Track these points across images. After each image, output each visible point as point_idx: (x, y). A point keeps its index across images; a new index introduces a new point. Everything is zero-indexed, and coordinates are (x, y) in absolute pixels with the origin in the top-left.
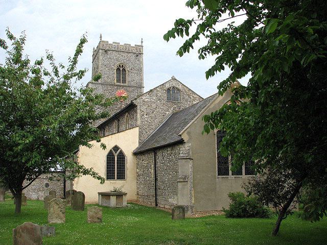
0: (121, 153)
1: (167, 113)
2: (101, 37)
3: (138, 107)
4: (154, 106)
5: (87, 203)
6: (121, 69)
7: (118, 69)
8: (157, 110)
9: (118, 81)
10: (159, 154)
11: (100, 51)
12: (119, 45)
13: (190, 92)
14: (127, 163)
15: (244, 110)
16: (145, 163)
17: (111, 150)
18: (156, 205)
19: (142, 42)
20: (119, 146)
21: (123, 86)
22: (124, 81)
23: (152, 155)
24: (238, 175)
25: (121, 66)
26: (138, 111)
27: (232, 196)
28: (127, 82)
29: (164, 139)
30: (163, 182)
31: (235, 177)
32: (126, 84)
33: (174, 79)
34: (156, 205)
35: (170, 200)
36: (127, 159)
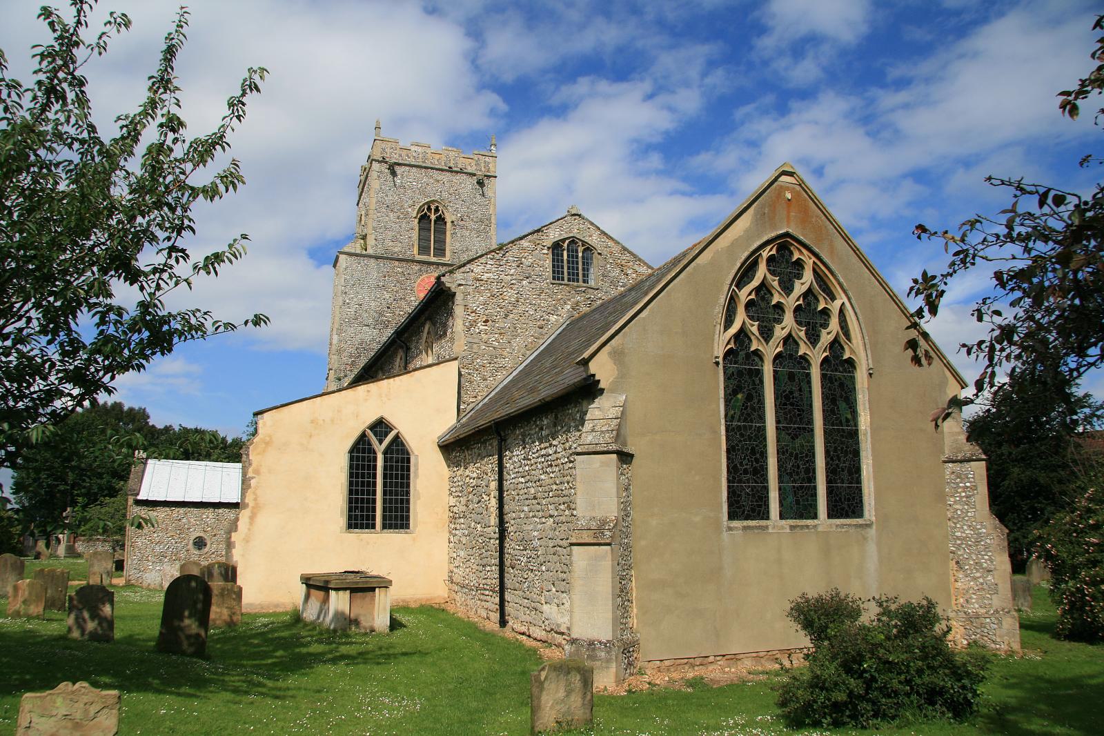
0: (398, 441)
1: (553, 318)
3: (459, 298)
4: (510, 295)
5: (214, 620)
6: (433, 217)
7: (424, 219)
8: (521, 308)
9: (424, 249)
11: (376, 166)
12: (428, 151)
13: (627, 257)
14: (416, 476)
16: (472, 471)
17: (363, 435)
18: (503, 622)
20: (391, 418)
22: (440, 251)
24: (801, 517)
25: (433, 207)
26: (458, 310)
28: (448, 253)
30: (525, 543)
31: (792, 527)
34: (503, 622)
35: (545, 608)
36: (416, 465)
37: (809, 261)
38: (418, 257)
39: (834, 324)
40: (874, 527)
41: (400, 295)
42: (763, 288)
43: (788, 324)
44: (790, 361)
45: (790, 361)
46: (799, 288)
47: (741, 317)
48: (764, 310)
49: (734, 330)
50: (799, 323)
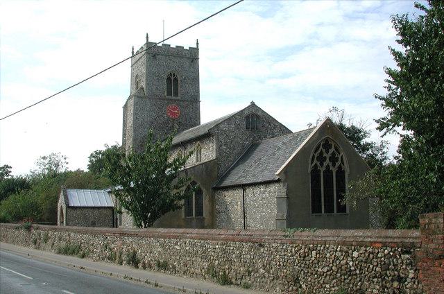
2: (147, 37)
7: (169, 79)
9: (169, 93)
10: (249, 191)
15: (110, 249)
19: (197, 44)
21: (175, 101)
22: (176, 94)
23: (241, 191)
27: (398, 65)
29: (254, 176)
32: (179, 98)
33: (253, 104)
37: (333, 145)
38: (167, 97)
39: (333, 148)
40: (204, 190)
41: (160, 114)
42: (321, 152)
43: (327, 162)
44: (328, 173)
45: (328, 173)
46: (331, 151)
47: (315, 161)
48: (321, 159)
49: (314, 164)
50: (330, 161)
